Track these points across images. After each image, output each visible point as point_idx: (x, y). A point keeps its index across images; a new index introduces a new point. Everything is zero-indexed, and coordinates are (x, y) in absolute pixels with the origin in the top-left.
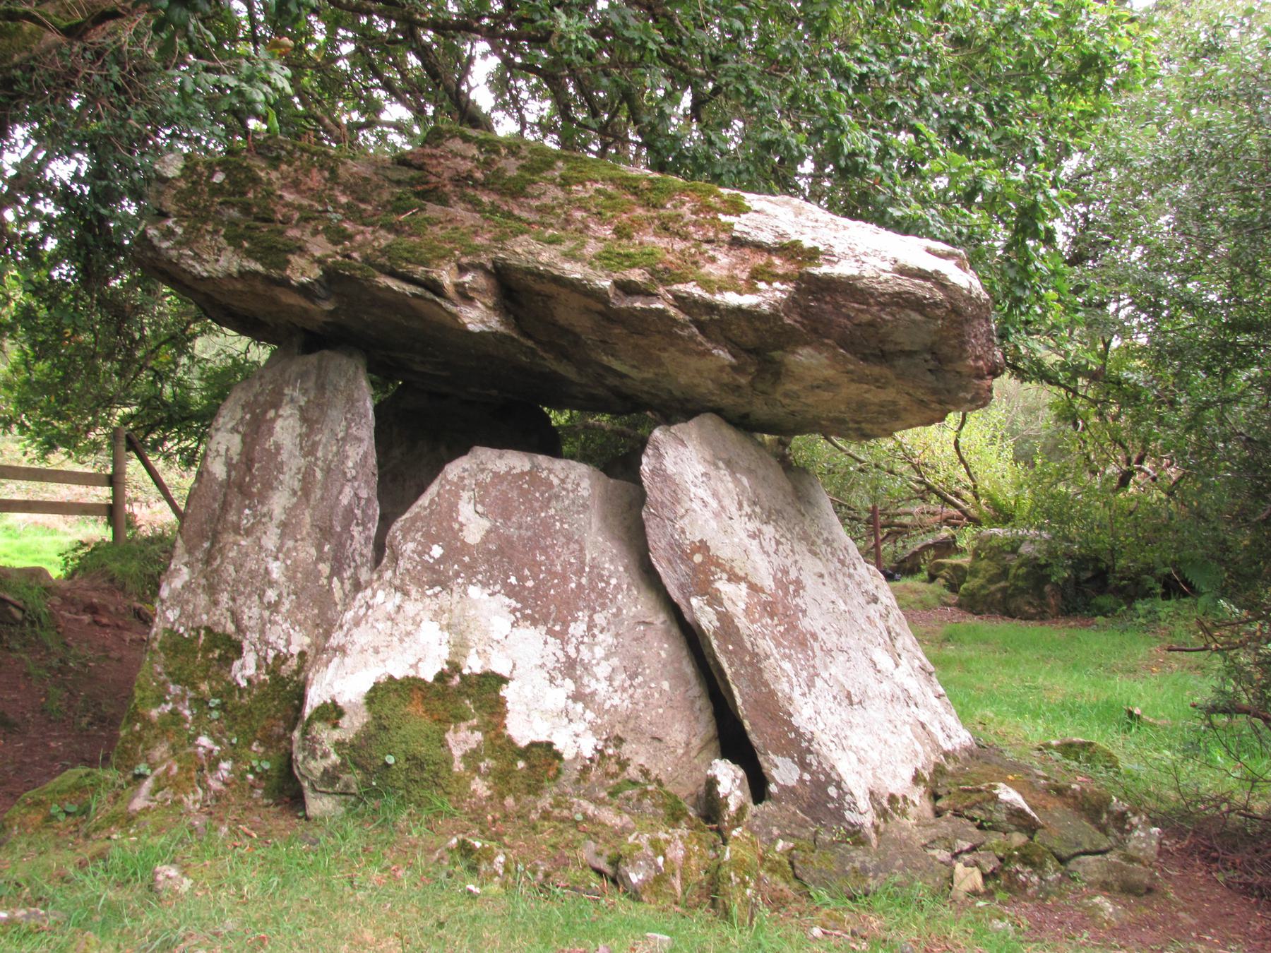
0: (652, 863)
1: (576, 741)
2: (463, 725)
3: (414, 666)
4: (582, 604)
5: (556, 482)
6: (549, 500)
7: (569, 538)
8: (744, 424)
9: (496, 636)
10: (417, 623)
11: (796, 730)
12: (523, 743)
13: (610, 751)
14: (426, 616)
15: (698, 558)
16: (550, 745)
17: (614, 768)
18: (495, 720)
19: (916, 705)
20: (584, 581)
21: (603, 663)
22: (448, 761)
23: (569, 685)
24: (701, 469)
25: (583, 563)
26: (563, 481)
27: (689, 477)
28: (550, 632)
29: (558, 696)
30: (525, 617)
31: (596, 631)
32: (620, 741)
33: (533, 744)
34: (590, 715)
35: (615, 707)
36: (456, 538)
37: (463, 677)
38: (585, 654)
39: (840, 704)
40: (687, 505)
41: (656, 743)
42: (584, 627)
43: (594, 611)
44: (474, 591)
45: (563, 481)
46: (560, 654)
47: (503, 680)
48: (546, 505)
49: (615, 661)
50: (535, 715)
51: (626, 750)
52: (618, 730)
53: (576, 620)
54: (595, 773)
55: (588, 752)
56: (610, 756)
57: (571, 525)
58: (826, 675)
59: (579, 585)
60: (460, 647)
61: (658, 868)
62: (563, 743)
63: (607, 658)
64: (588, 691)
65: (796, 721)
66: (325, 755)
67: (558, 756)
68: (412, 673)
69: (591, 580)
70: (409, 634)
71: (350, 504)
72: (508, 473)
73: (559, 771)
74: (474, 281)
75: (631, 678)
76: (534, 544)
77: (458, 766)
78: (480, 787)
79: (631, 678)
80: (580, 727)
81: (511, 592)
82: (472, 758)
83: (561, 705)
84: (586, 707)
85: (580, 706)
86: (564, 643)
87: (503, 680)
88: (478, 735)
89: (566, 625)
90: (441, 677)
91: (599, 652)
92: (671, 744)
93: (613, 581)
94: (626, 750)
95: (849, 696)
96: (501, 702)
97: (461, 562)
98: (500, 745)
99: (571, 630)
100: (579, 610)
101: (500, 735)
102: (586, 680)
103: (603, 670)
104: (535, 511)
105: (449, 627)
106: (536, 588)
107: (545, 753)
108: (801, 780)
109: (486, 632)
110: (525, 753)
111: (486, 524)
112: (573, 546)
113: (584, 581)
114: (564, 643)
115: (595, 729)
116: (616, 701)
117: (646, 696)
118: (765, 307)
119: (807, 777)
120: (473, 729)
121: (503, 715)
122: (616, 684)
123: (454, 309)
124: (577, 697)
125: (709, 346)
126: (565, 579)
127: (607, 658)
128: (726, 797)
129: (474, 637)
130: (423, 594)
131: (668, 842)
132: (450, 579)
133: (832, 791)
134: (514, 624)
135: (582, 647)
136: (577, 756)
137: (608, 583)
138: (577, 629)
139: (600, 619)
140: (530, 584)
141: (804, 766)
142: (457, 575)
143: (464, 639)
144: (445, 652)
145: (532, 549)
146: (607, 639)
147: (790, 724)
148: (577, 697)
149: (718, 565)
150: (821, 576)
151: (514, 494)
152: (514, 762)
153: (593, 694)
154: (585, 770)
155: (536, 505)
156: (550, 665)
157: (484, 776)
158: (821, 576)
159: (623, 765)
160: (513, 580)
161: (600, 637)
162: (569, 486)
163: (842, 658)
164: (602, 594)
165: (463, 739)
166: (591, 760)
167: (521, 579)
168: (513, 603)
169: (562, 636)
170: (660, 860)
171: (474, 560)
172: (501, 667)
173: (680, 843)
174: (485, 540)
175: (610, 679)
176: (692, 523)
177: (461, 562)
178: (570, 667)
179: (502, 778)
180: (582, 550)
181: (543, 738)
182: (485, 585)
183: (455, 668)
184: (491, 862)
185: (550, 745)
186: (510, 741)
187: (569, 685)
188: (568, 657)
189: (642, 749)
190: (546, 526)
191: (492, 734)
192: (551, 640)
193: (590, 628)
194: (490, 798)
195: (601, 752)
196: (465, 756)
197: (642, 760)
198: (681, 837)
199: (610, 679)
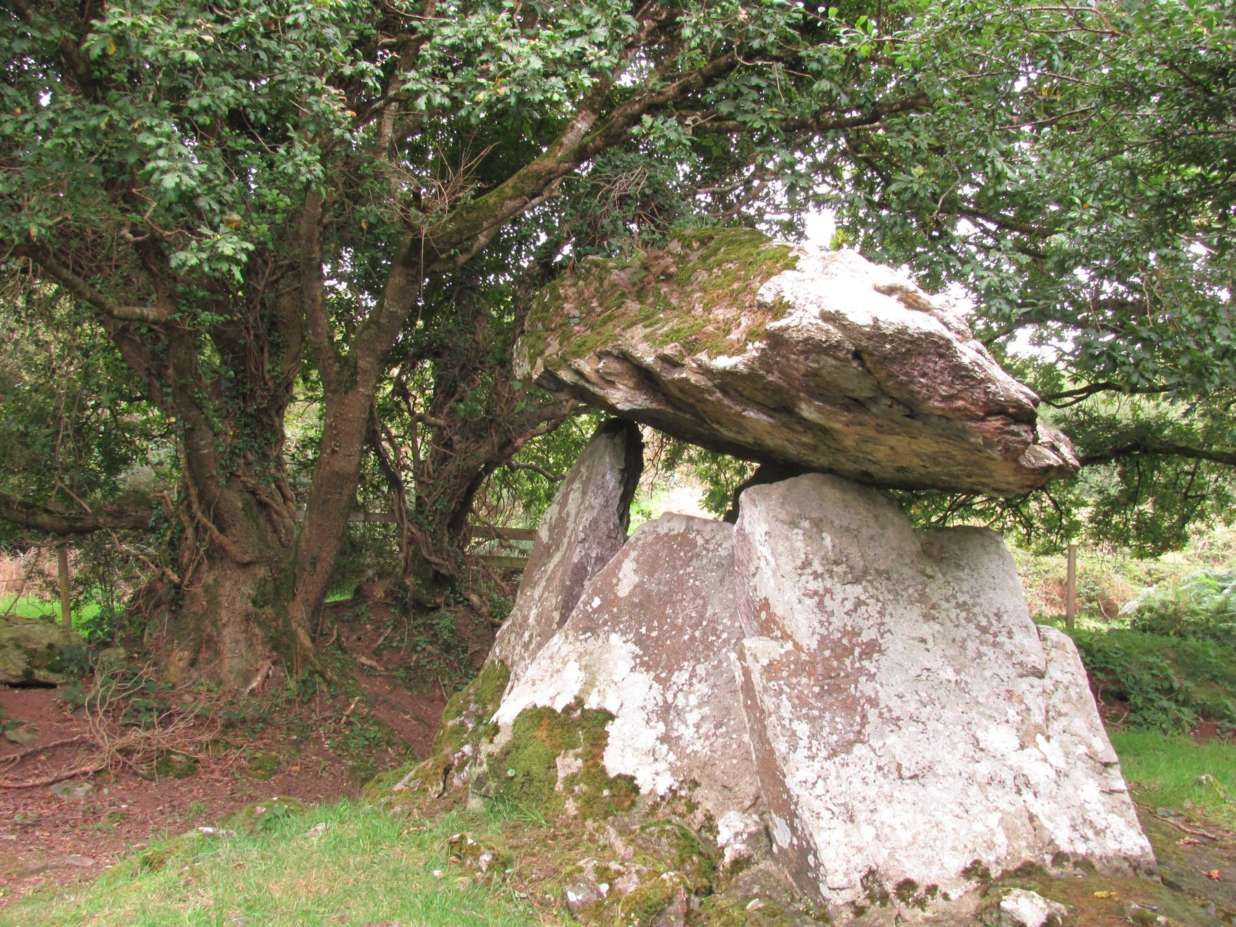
0: (593, 888)
1: (655, 779)
2: (571, 752)
3: (553, 699)
4: (689, 654)
5: (700, 541)
6: (691, 559)
7: (697, 595)
8: (867, 484)
9: (617, 678)
10: (565, 663)
11: (787, 791)
12: (612, 775)
13: (683, 793)
14: (574, 656)
15: (763, 615)
16: (633, 778)
17: (682, 808)
18: (595, 751)
19: (1035, 794)
20: (697, 634)
21: (696, 711)
22: (553, 781)
23: (661, 728)
24: (765, 528)
25: (702, 617)
26: (707, 542)
27: (757, 537)
28: (657, 679)
29: (649, 736)
30: (642, 664)
31: (695, 681)
32: (695, 784)
33: (619, 776)
34: (672, 757)
35: (696, 752)
36: (612, 591)
37: (583, 711)
38: (681, 701)
39: (885, 776)
40: (756, 563)
41: (726, 792)
42: (687, 676)
43: (698, 661)
44: (615, 638)
45: (707, 542)
46: (660, 699)
47: (611, 717)
48: (687, 563)
49: (706, 710)
50: (629, 750)
51: (699, 794)
52: (695, 775)
53: (681, 669)
54: (663, 811)
55: (661, 790)
56: (681, 797)
57: (702, 582)
58: (876, 743)
59: (693, 638)
60: (589, 684)
61: (600, 894)
62: (644, 782)
63: (699, 706)
64: (675, 734)
65: (790, 782)
66: (481, 764)
67: (636, 789)
68: (549, 704)
69: (704, 633)
70: (558, 671)
71: (580, 561)
72: (666, 534)
73: (633, 803)
74: (606, 365)
75: (716, 727)
76: (668, 599)
77: (559, 787)
78: (571, 807)
79: (716, 727)
80: (661, 766)
81: (639, 641)
82: (571, 780)
83: (650, 745)
84: (670, 749)
85: (666, 747)
86: (666, 688)
87: (611, 717)
88: (580, 762)
89: (671, 672)
90: (568, 709)
91: (693, 700)
92: (739, 794)
93: (724, 636)
94: (699, 794)
95: (899, 767)
96: (606, 735)
97: (610, 612)
98: (595, 771)
99: (674, 678)
100: (685, 659)
101: (596, 765)
102: (675, 725)
103: (693, 718)
104: (675, 568)
105: (586, 667)
106: (657, 638)
107: (628, 785)
108: (791, 844)
109: (611, 674)
110: (613, 783)
111: (636, 579)
112: (700, 602)
113: (697, 634)
114: (666, 688)
115: (673, 770)
116: (698, 747)
117: (724, 746)
118: (741, 367)
119: (795, 842)
120: (577, 756)
121: (603, 746)
122: (702, 731)
123: (600, 392)
124: (664, 739)
125: (739, 409)
126: (681, 630)
127: (699, 706)
128: (723, 848)
129: (601, 678)
130: (577, 638)
131: (619, 874)
132: (599, 626)
133: (811, 859)
134: (633, 669)
135: (680, 695)
136: (652, 792)
137: (719, 637)
138: (680, 677)
139: (701, 670)
140: (654, 634)
141: (794, 830)
142: (605, 623)
143: (594, 678)
144: (575, 689)
145: (666, 603)
146: (703, 688)
147: (783, 784)
148: (664, 739)
149: (775, 623)
150: (923, 641)
151: (663, 554)
152: (600, 790)
153: (679, 738)
154: (655, 806)
155: (678, 563)
156: (650, 708)
157: (576, 798)
158: (923, 641)
159: (692, 807)
160: (643, 630)
161: (698, 686)
162: (711, 547)
163: (914, 728)
164: (709, 646)
165: (569, 764)
166: (663, 798)
167: (650, 629)
168: (638, 651)
169: (664, 683)
170: (604, 888)
171: (620, 610)
172: (612, 708)
173: (635, 878)
174: (631, 594)
175: (698, 726)
176: (761, 580)
177: (610, 612)
178: (666, 712)
179: (589, 803)
180: (704, 605)
181: (630, 773)
182: (624, 633)
183: (579, 702)
184: (477, 858)
185: (633, 778)
186: (603, 771)
187: (661, 728)
188: (665, 701)
189: (712, 795)
190: (681, 582)
191: (590, 763)
192: (655, 685)
193: (691, 677)
194: (575, 817)
195: (674, 792)
196: (566, 779)
197: (709, 805)
198: (638, 872)
199: (698, 726)
